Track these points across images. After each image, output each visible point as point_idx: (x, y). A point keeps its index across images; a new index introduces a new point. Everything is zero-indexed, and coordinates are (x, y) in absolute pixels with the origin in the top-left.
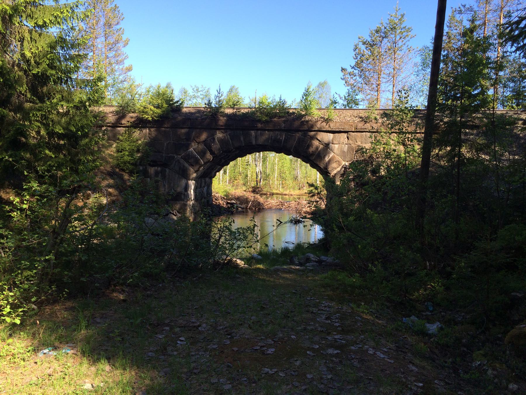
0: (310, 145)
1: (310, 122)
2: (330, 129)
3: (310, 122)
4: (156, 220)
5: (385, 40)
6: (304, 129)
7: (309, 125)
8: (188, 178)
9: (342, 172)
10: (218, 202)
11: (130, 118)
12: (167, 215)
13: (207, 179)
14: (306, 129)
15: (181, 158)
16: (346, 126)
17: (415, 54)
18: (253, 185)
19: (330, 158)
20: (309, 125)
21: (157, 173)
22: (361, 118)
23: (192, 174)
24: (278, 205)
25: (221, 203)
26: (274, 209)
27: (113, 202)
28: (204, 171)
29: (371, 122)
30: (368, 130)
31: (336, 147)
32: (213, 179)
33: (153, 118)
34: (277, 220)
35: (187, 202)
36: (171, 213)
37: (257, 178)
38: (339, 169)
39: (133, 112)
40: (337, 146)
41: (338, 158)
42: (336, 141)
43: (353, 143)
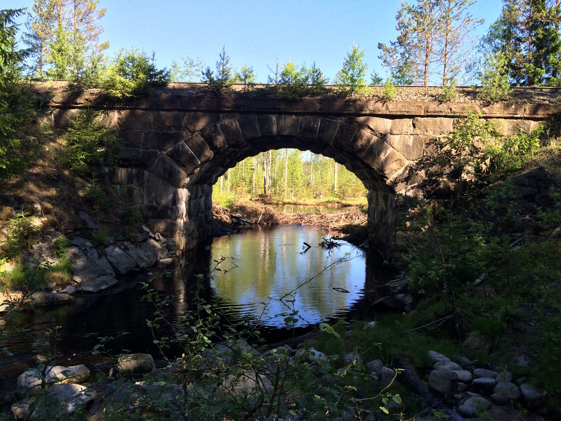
0: (359, 136)
1: (359, 102)
2: (388, 113)
3: (359, 102)
4: (126, 249)
5: (437, 8)
6: (350, 112)
7: (358, 107)
8: (177, 184)
9: (406, 175)
10: (219, 216)
11: (89, 94)
12: (145, 240)
13: (205, 186)
14: (352, 112)
15: (167, 154)
16: (411, 108)
17: (474, 26)
18: (260, 193)
19: (387, 154)
20: (358, 107)
21: (130, 178)
22: (433, 96)
23: (184, 179)
24: (296, 219)
25: (223, 217)
26: (290, 225)
27: (52, 224)
28: (200, 174)
29: (448, 102)
30: (444, 114)
31: (395, 140)
32: (214, 186)
33: (124, 95)
34: (305, 243)
35: (176, 219)
36: (151, 237)
37: (265, 184)
38: (400, 171)
39: (95, 87)
40: (397, 138)
41: (399, 155)
42: (396, 130)
43: (422, 132)
